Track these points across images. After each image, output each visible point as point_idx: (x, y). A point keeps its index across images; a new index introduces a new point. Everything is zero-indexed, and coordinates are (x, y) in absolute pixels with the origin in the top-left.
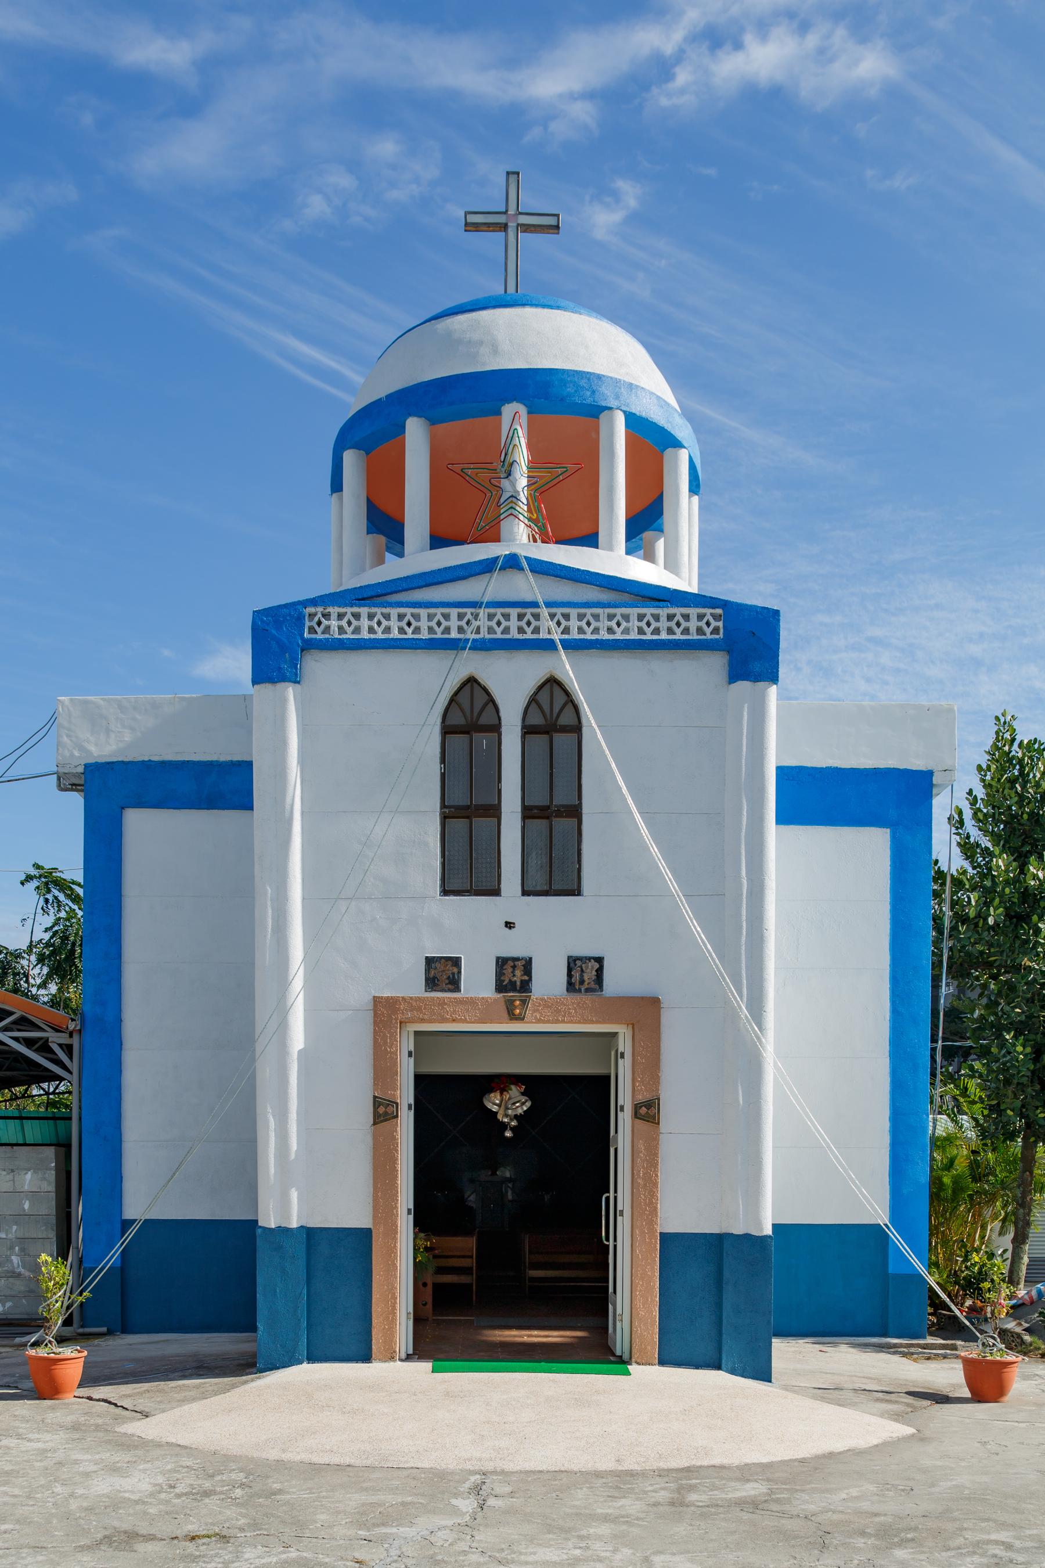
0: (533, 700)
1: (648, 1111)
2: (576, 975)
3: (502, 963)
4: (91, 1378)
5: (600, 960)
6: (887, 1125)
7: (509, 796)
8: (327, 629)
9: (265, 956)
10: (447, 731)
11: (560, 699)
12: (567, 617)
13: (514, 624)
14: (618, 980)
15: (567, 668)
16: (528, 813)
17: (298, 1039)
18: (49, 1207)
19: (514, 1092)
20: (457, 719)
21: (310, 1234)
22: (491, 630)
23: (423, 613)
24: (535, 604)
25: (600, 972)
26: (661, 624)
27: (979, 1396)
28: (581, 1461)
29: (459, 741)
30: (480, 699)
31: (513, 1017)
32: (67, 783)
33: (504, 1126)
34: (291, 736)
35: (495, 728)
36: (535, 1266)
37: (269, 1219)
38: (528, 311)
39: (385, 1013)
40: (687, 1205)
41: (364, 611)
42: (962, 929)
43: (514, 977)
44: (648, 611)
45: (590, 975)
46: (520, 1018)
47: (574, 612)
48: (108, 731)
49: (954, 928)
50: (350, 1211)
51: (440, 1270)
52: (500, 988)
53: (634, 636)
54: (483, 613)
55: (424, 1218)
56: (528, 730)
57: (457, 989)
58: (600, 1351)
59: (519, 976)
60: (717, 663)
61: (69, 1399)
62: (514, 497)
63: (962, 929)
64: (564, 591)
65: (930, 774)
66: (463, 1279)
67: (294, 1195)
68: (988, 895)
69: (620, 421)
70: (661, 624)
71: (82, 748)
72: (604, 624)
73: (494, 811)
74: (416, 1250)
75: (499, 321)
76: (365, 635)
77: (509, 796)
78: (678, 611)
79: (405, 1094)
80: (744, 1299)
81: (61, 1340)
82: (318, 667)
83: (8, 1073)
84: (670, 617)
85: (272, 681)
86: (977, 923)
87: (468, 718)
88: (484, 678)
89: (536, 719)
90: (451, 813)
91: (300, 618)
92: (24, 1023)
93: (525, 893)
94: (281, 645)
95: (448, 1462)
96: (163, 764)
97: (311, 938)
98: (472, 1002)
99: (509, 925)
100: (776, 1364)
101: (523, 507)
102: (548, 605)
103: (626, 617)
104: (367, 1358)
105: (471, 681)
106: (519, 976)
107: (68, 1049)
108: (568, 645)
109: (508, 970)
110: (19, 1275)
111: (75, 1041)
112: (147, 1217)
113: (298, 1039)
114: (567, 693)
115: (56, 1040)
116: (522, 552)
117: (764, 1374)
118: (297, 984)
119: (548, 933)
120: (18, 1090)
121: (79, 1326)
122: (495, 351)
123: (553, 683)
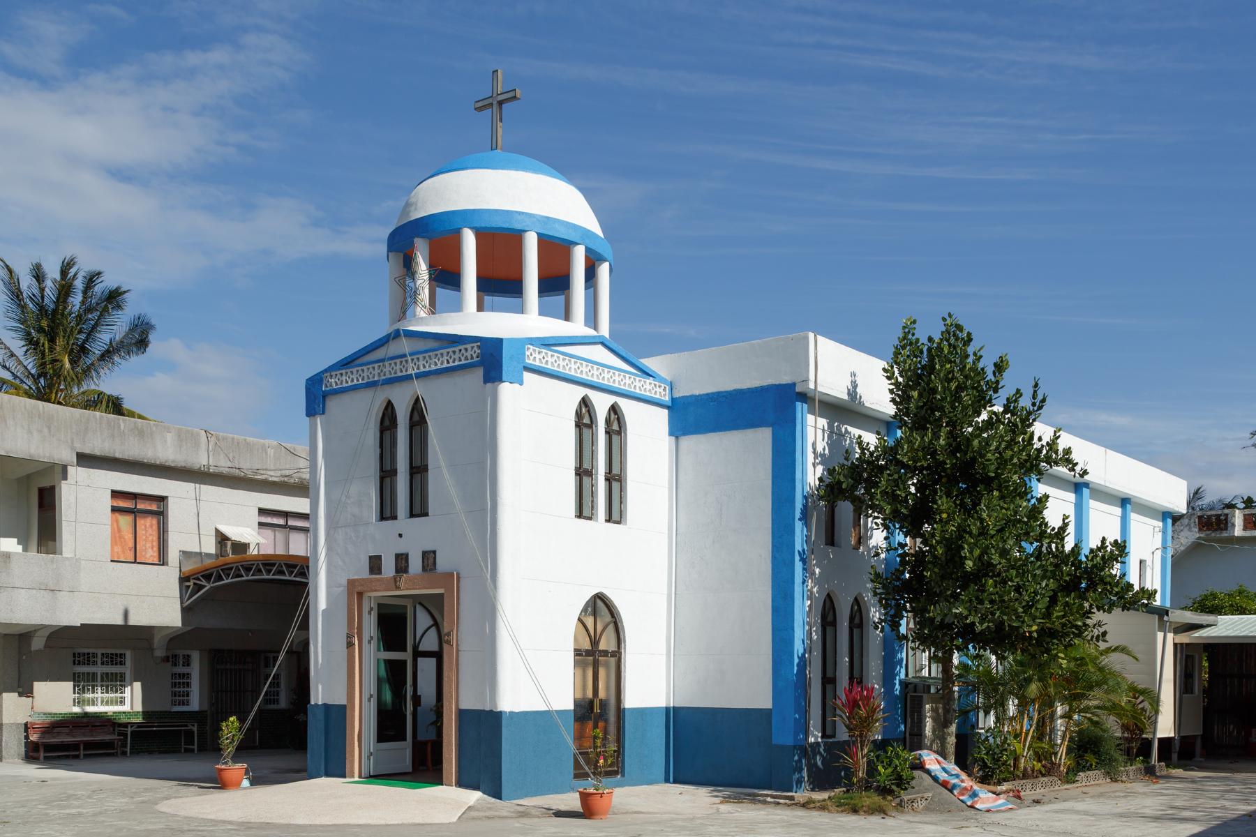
5: (434, 552)
14: (443, 564)
24: (405, 356)
43: (402, 561)
47: (421, 356)
53: (445, 365)
54: (386, 364)
82: (333, 404)
102: (411, 355)
119: (413, 536)
121: (245, 749)
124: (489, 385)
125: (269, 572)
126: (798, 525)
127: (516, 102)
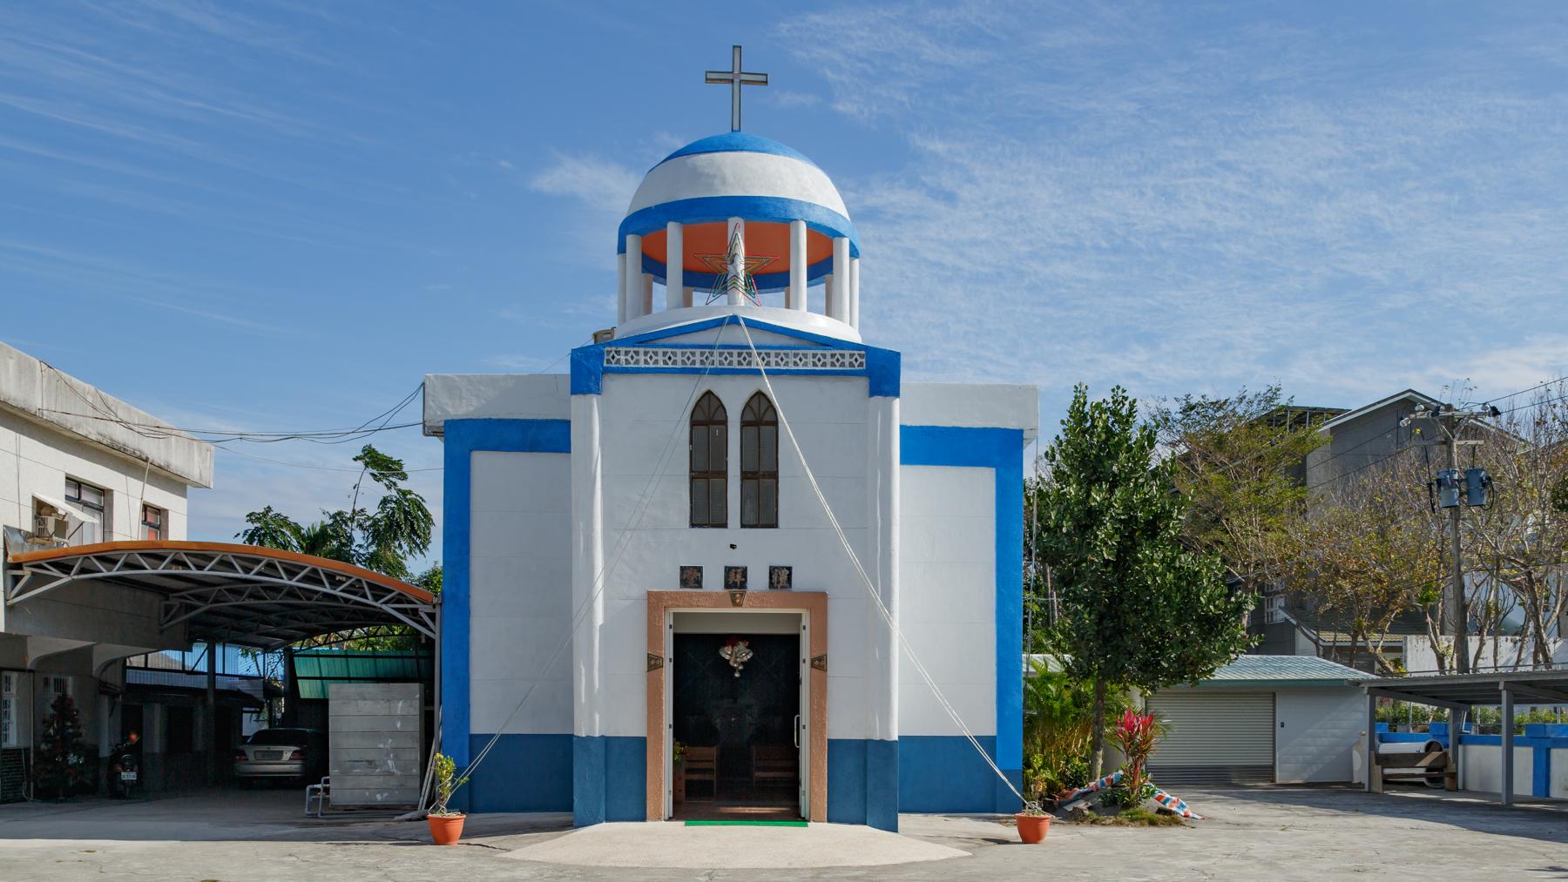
0: (748, 405)
1: (820, 663)
2: (775, 578)
3: (728, 570)
4: (467, 834)
5: (789, 569)
6: (994, 668)
7: (733, 465)
8: (618, 361)
9: (578, 565)
10: (694, 423)
11: (764, 405)
12: (768, 355)
13: (735, 359)
14: (800, 582)
15: (768, 386)
16: (745, 476)
17: (599, 619)
18: (415, 726)
19: (742, 646)
20: (700, 417)
21: (607, 741)
22: (721, 363)
23: (679, 352)
25: (790, 575)
26: (827, 360)
27: (1026, 840)
28: (770, 864)
29: (701, 429)
30: (714, 404)
31: (735, 604)
32: (430, 431)
33: (734, 670)
34: (592, 420)
35: (724, 422)
36: (759, 769)
37: (581, 731)
38: (745, 154)
39: (655, 601)
40: (844, 723)
41: (641, 350)
42: (1045, 535)
43: (736, 579)
44: (819, 352)
45: (784, 577)
46: (740, 605)
47: (773, 352)
48: (461, 398)
49: (1039, 535)
50: (631, 724)
51: (688, 771)
52: (727, 586)
53: (810, 367)
54: (716, 352)
55: (679, 734)
56: (745, 424)
57: (700, 586)
58: (795, 815)
59: (739, 578)
60: (862, 384)
61: (455, 843)
62: (736, 276)
63: (1045, 535)
64: (768, 339)
65: (1021, 431)
66: (707, 777)
67: (597, 717)
68: (1065, 511)
69: (803, 227)
70: (827, 360)
71: (442, 410)
72: (791, 360)
73: (723, 474)
74: (674, 752)
75: (726, 161)
76: (642, 365)
77: (733, 465)
78: (838, 352)
79: (668, 651)
80: (884, 781)
81: (450, 807)
82: (612, 384)
83: (252, 602)
84: (833, 356)
85: (584, 393)
86: (1053, 531)
87: (707, 415)
88: (716, 391)
89: (750, 417)
90: (696, 476)
91: (601, 355)
92: (400, 599)
93: (743, 526)
94: (588, 370)
95: (694, 864)
96: (500, 421)
97: (608, 554)
98: (709, 595)
99: (733, 546)
100: (900, 824)
101: (742, 282)
103: (805, 356)
104: (643, 819)
105: (709, 393)
106: (739, 578)
107: (432, 616)
108: (768, 372)
109: (732, 574)
110: (393, 774)
111: (437, 611)
112: (506, 732)
113: (599, 619)
114: (769, 401)
115: (423, 610)
116: (742, 314)
117: (895, 830)
118: (599, 584)
119: (757, 551)
120: (346, 633)
121: (465, 801)
122: (724, 182)
123: (760, 395)
124: (878, 399)
125: (247, 570)
126: (205, 572)
127: (763, 87)
